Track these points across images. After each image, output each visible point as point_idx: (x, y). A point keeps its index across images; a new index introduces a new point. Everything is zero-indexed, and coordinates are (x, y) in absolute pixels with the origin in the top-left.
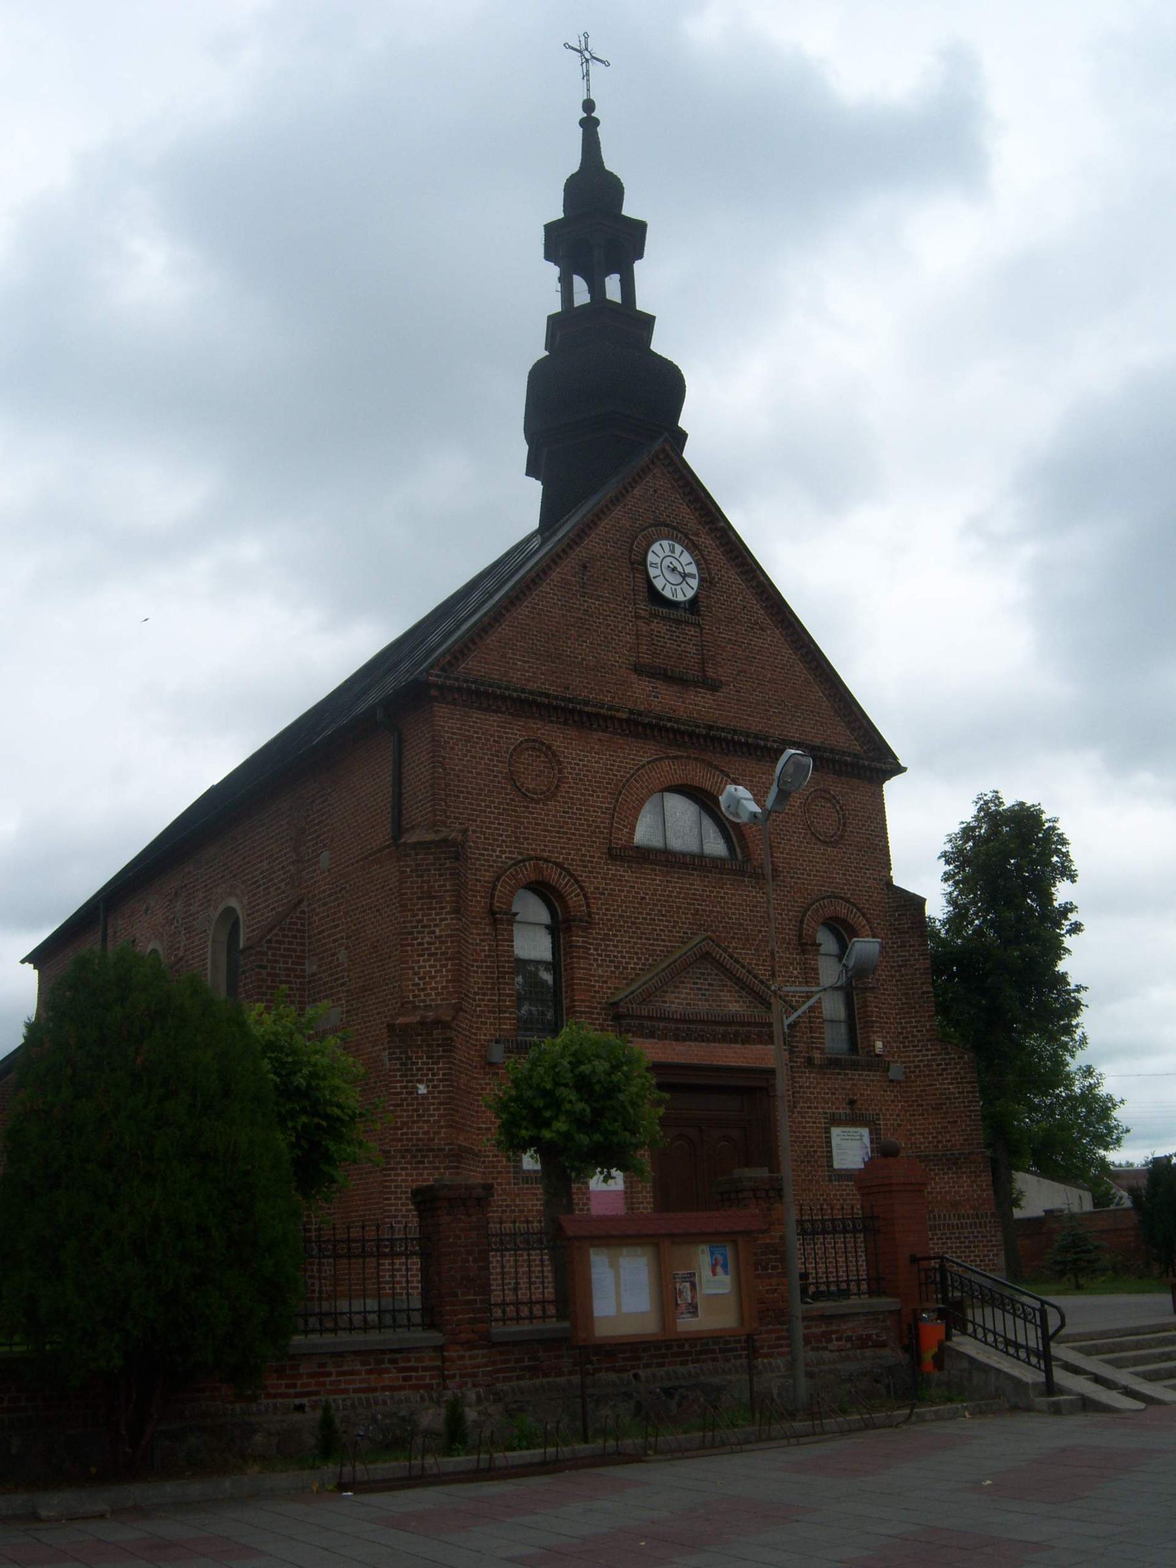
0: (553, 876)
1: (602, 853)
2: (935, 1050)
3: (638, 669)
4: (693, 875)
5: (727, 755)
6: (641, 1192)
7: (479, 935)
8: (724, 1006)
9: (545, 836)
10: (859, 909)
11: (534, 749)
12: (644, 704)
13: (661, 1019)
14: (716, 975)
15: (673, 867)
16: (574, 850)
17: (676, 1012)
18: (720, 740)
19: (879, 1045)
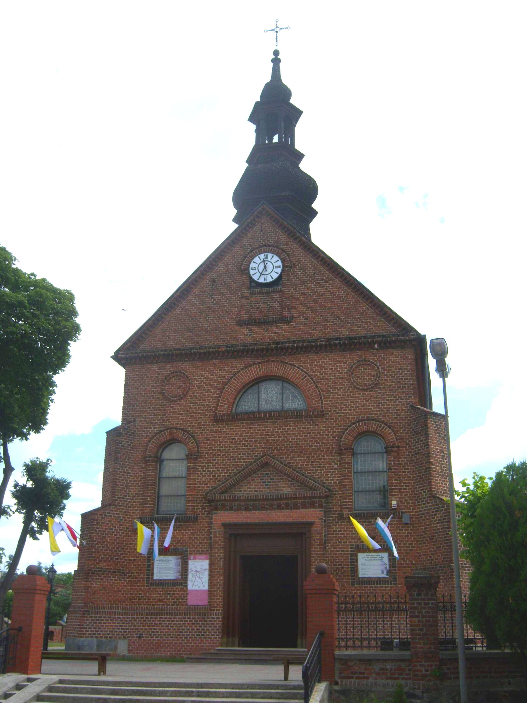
0: (362, 427)
1: (211, 420)
2: (432, 503)
3: (240, 323)
4: (268, 422)
5: (295, 355)
6: (216, 591)
7: (138, 469)
8: (280, 490)
9: (179, 417)
10: (386, 424)
11: (177, 376)
12: (243, 340)
13: (236, 500)
14: (276, 473)
15: (254, 420)
16: (194, 421)
17: (243, 496)
18: (287, 349)
19: (394, 503)
